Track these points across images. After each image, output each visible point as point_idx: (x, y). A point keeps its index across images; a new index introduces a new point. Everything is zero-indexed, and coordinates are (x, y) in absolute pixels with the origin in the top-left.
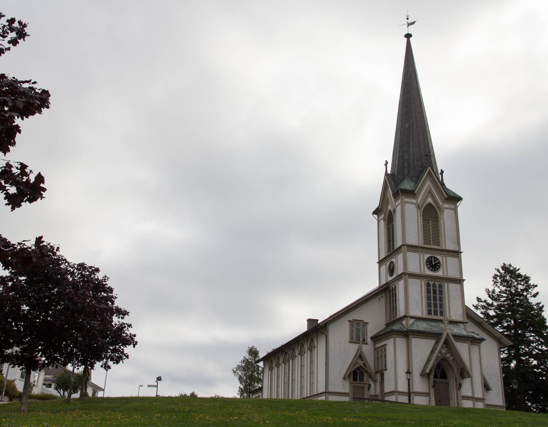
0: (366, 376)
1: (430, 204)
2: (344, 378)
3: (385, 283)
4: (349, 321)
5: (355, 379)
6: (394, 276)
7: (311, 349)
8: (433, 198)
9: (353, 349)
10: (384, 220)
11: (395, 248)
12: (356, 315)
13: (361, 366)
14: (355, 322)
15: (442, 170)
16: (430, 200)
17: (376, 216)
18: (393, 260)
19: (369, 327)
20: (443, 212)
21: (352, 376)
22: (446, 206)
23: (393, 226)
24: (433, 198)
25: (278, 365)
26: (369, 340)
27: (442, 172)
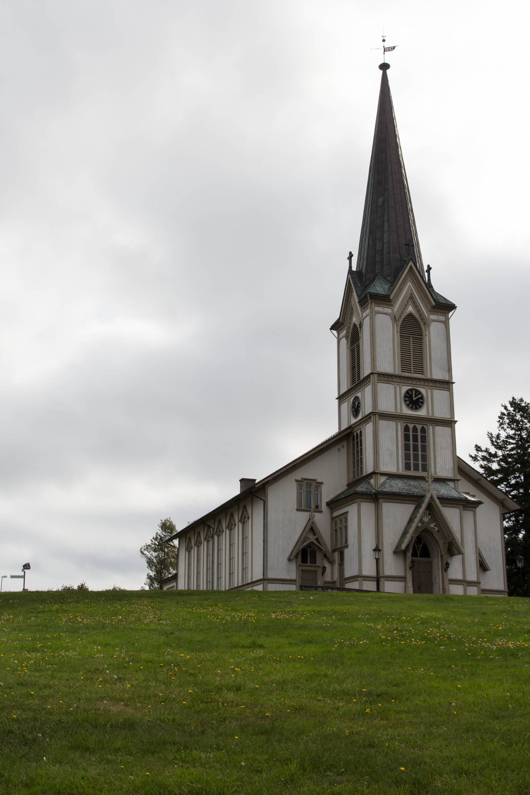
0: (319, 556)
1: (410, 315)
2: (289, 560)
4: (296, 481)
5: (304, 560)
6: (360, 417)
7: (244, 520)
8: (416, 306)
9: (302, 518)
11: (362, 378)
13: (312, 542)
14: (305, 481)
15: (428, 266)
16: (410, 309)
17: (335, 332)
18: (359, 395)
19: (324, 489)
20: (429, 326)
22: (433, 317)
23: (358, 347)
24: (416, 306)
26: (324, 507)
27: (429, 268)
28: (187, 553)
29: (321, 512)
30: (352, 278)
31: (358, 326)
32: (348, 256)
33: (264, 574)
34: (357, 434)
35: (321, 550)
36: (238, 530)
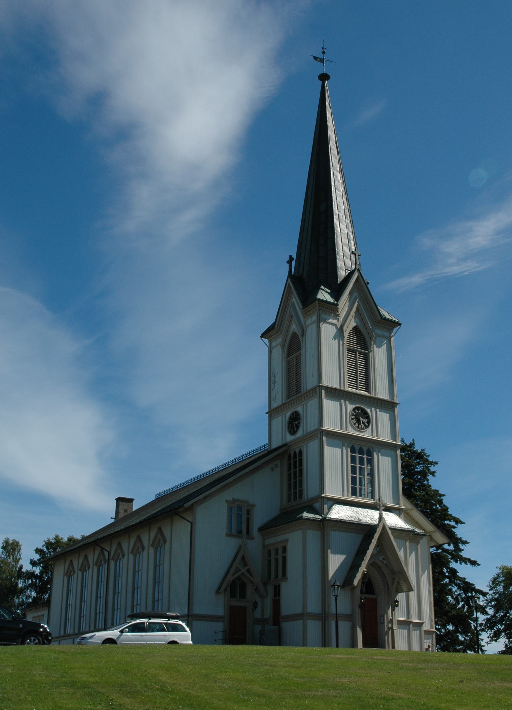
0: (250, 590)
2: (218, 592)
3: (280, 444)
4: (227, 501)
5: (233, 595)
6: (300, 433)
7: (159, 543)
9: (233, 543)
10: (283, 346)
12: (239, 492)
17: (266, 340)
18: (299, 409)
21: (229, 589)
22: (378, 331)
25: (84, 569)
26: (255, 531)
28: (66, 578)
29: (252, 538)
30: (293, 283)
31: (300, 335)
32: (288, 259)
33: (188, 610)
34: (295, 453)
35: (253, 583)
36: (147, 556)
